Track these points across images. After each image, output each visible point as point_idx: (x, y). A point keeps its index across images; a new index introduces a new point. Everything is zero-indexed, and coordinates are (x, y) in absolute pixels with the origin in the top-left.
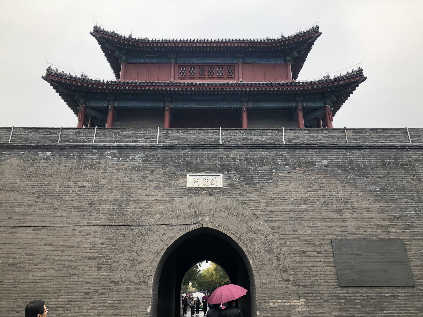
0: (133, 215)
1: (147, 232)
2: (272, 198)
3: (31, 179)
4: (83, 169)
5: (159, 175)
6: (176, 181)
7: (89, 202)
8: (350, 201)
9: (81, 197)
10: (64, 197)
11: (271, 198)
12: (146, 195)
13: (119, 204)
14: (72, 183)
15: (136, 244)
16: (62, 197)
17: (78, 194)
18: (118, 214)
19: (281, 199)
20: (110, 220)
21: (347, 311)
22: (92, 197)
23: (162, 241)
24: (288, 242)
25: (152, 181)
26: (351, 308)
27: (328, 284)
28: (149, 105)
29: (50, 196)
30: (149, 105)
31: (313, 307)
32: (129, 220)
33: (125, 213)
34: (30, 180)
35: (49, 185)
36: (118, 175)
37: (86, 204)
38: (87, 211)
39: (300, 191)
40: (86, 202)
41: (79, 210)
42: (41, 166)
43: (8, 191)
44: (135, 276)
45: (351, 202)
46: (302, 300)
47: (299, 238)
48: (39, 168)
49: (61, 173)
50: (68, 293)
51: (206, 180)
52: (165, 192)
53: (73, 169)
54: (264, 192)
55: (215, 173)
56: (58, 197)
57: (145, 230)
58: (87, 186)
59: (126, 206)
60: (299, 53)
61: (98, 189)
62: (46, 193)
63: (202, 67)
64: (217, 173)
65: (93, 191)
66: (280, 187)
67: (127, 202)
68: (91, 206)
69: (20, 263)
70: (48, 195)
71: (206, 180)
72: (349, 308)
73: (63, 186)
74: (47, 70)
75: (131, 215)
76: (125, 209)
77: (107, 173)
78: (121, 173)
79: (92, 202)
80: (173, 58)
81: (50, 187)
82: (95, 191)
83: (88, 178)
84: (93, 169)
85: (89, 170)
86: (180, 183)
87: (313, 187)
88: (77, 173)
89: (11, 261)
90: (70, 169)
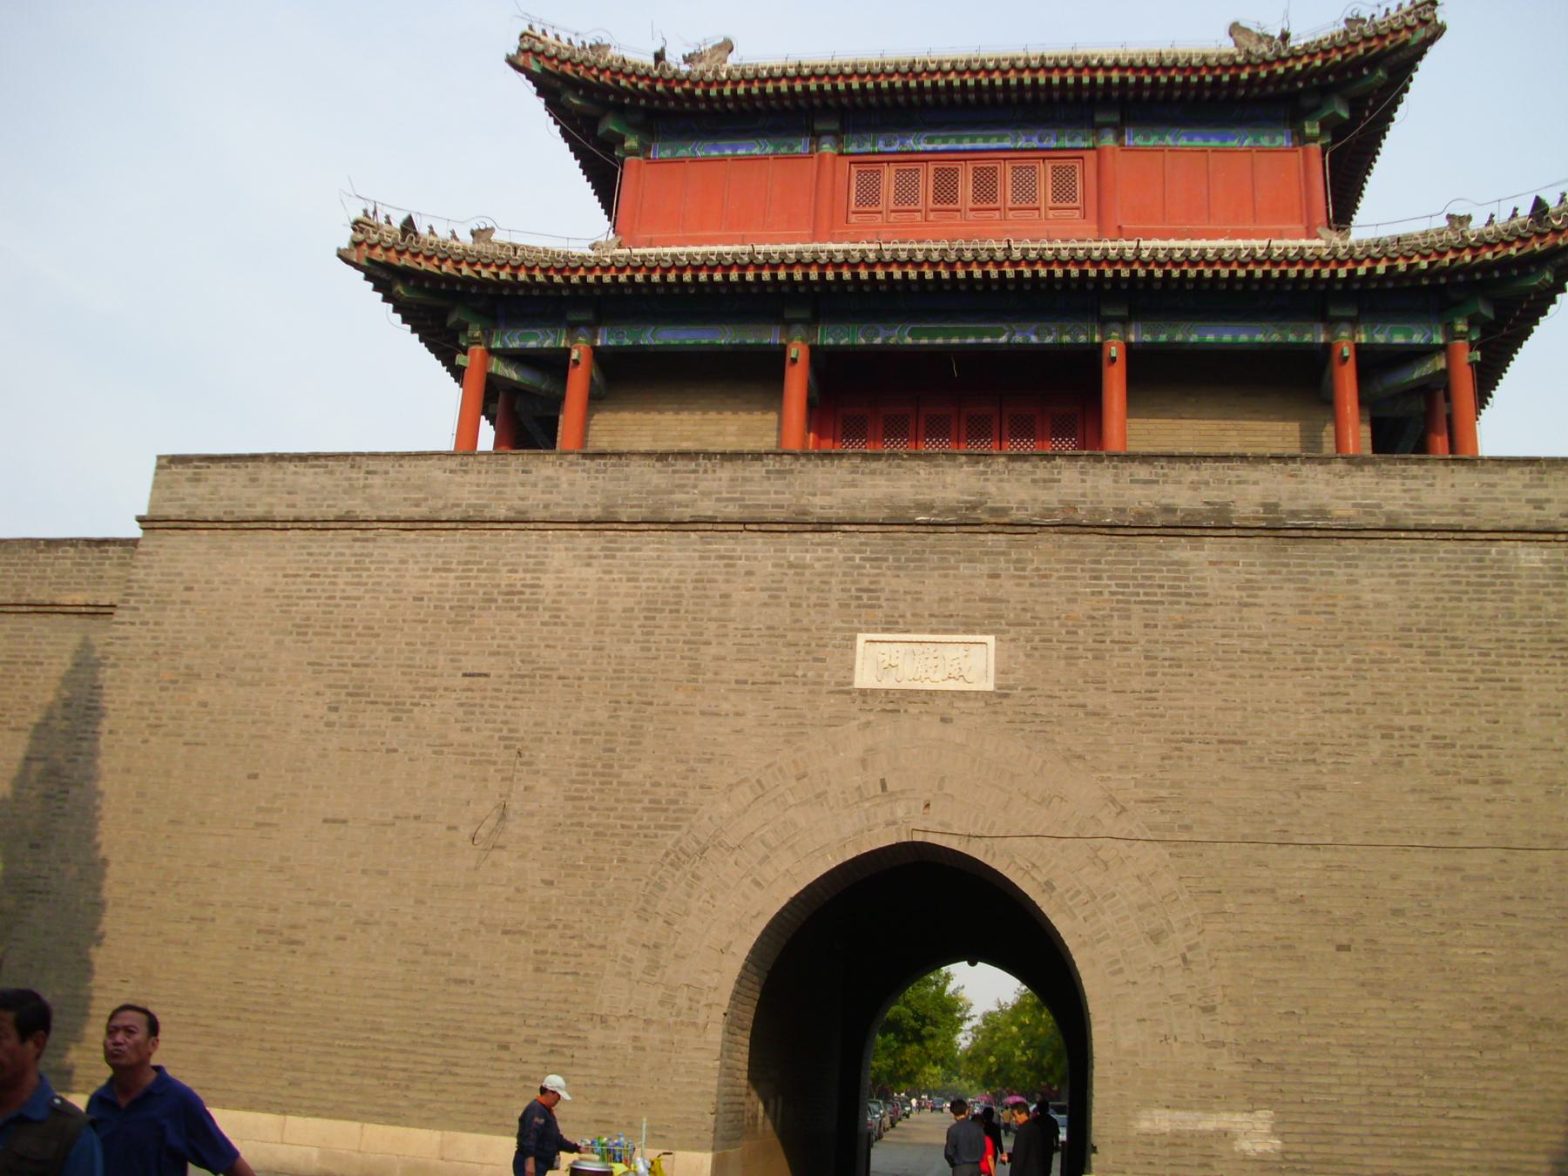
0: (656, 784)
1: (704, 850)
2: (1187, 735)
3: (311, 641)
4: (480, 608)
5: (751, 636)
6: (816, 660)
7: (501, 730)
8: (1488, 751)
9: (473, 713)
10: (416, 709)
11: (1179, 737)
12: (703, 713)
13: (606, 741)
14: (442, 660)
15: (664, 889)
16: (411, 711)
17: (463, 700)
18: (602, 779)
19: (1220, 742)
20: (574, 799)
21: (1422, 1157)
22: (512, 714)
23: (757, 884)
24: (1230, 907)
25: (724, 659)
26: (1442, 1147)
27: (1363, 1061)
28: (723, 337)
29: (372, 703)
30: (723, 337)
31: (1297, 1139)
32: (640, 801)
33: (626, 775)
34: (306, 646)
35: (367, 665)
36: (602, 633)
37: (491, 737)
38: (495, 763)
39: (1297, 713)
40: (491, 730)
41: (469, 759)
42: (338, 594)
43: (241, 683)
44: (662, 1003)
45: (1490, 756)
46: (1260, 1114)
47: (1273, 891)
48: (333, 602)
49: (404, 621)
50: (445, 1036)
51: (931, 659)
52: (772, 705)
53: (444, 608)
54: (1155, 711)
55: (965, 632)
56: (398, 709)
57: (698, 842)
58: (493, 673)
59: (629, 752)
60: (1356, 105)
61: (532, 684)
62: (357, 695)
63: (946, 165)
64: (973, 632)
65: (514, 692)
66: (1219, 692)
67: (633, 736)
68: (506, 747)
69: (294, 927)
70: (364, 699)
71: (931, 659)
72: (1433, 1147)
73: (414, 671)
74: (357, 225)
75: (648, 784)
76: (626, 762)
77: (563, 624)
78: (613, 625)
79: (511, 731)
80: (827, 133)
81: (369, 670)
82: (521, 692)
83: (496, 642)
84: (512, 609)
85: (499, 613)
86: (827, 669)
87: (1347, 694)
88: (459, 622)
89: (263, 917)
90: (436, 607)
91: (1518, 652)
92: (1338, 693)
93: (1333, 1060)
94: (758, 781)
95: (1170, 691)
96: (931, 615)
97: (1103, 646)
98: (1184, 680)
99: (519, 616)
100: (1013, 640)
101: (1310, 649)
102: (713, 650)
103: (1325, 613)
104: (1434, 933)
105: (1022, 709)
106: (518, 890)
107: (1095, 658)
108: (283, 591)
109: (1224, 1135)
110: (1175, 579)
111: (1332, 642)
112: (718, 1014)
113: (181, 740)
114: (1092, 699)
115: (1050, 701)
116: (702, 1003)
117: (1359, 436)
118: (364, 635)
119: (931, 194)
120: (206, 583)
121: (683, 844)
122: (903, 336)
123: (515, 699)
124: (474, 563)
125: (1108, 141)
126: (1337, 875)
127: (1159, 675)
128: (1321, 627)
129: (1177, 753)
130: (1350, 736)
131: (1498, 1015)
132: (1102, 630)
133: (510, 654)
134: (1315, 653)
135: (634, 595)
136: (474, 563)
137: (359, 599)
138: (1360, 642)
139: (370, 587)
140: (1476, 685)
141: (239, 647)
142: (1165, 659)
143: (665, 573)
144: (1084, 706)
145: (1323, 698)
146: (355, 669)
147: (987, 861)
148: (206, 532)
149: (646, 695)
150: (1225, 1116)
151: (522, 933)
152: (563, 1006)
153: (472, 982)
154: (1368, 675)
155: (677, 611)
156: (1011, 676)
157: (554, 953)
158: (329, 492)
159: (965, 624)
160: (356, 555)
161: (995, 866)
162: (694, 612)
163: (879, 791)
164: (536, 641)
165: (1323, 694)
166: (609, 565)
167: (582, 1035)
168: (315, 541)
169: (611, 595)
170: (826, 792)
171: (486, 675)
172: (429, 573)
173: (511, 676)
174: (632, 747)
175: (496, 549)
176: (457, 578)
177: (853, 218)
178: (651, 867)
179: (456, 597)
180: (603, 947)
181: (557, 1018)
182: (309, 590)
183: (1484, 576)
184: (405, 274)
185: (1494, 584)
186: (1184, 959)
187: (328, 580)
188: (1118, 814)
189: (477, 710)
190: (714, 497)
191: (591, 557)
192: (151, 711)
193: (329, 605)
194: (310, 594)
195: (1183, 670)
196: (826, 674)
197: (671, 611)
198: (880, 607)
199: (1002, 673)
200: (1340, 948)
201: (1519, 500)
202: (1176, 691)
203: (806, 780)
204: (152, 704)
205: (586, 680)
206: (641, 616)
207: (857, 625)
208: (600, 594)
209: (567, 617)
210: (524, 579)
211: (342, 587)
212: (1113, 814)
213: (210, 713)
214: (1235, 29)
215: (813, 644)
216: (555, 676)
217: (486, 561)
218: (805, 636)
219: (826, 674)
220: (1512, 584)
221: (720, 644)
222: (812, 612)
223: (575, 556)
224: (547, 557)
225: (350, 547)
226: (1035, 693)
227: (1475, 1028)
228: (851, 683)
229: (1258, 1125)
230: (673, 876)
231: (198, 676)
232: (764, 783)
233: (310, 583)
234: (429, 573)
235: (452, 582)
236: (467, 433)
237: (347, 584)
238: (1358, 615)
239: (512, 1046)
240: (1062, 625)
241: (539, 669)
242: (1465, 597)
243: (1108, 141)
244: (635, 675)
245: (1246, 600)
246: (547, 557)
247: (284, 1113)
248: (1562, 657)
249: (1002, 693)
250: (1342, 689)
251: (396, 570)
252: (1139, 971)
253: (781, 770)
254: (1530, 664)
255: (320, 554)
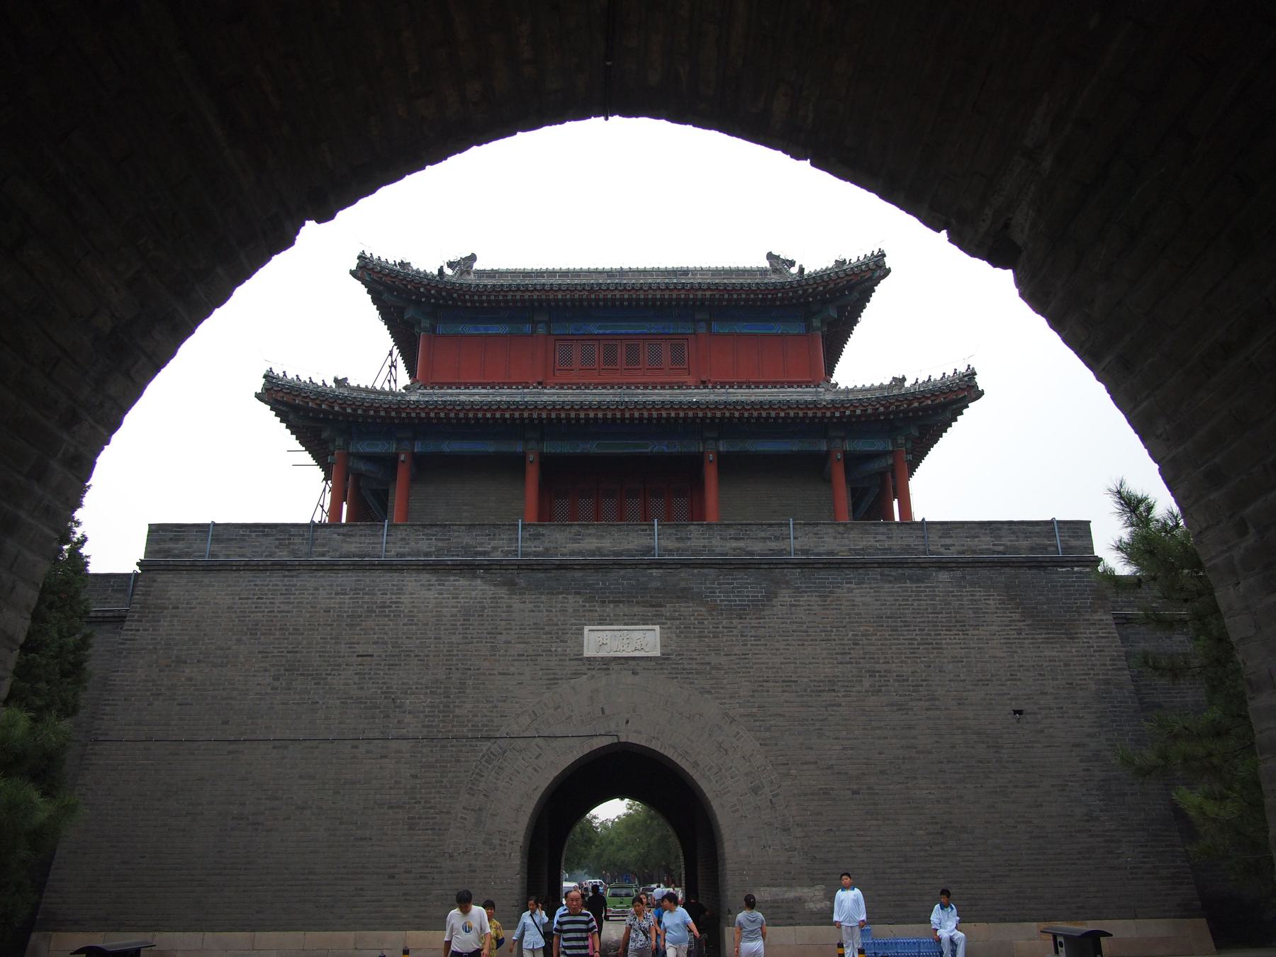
1: (505, 752)
2: (765, 678)
3: (260, 638)
6: (562, 641)
7: (382, 688)
10: (329, 677)
11: (761, 679)
12: (500, 674)
15: (483, 776)
17: (359, 671)
19: (783, 681)
25: (510, 642)
28: (490, 447)
29: (301, 675)
30: (490, 447)
32: (466, 726)
33: (458, 711)
35: (296, 652)
37: (376, 692)
39: (824, 664)
40: (375, 688)
42: (276, 610)
46: (818, 887)
47: (816, 763)
48: (273, 614)
54: (747, 665)
55: (643, 624)
57: (501, 748)
58: (375, 654)
59: (458, 698)
60: (841, 310)
62: (292, 670)
65: (389, 665)
68: (386, 698)
76: (457, 704)
77: (416, 625)
78: (445, 624)
79: (388, 688)
81: (299, 655)
82: (393, 665)
84: (385, 616)
85: (377, 619)
88: (353, 625)
91: (939, 628)
92: (845, 653)
93: (855, 855)
94: (533, 711)
95: (756, 654)
96: (624, 615)
97: (718, 630)
98: (762, 648)
99: (389, 620)
100: (669, 628)
101: (829, 629)
102: (503, 638)
103: (836, 609)
104: (903, 783)
105: (676, 666)
106: (396, 782)
107: (714, 637)
108: (238, 608)
109: (799, 900)
110: (755, 592)
111: (840, 625)
112: (517, 847)
113: (175, 703)
114: (714, 659)
115: (691, 662)
116: (508, 841)
117: (845, 517)
118: (294, 634)
119: (602, 359)
120: (187, 604)
121: (493, 750)
122: (592, 448)
123: (389, 669)
124: (360, 590)
125: (702, 330)
126: (850, 752)
127: (749, 645)
128: (834, 617)
129: (761, 688)
130: (853, 676)
131: (939, 826)
132: (717, 621)
133: (386, 643)
134: (832, 631)
135: (457, 607)
136: (360, 590)
137: (288, 612)
138: (856, 625)
139: (295, 605)
140: (918, 646)
141: (211, 643)
142: (752, 636)
143: (474, 593)
144: (709, 664)
145: (837, 656)
146: (289, 655)
147: (662, 751)
148: (185, 572)
149: (467, 664)
150: (799, 889)
151: (399, 807)
152: (427, 849)
153: (371, 839)
154: (861, 642)
155: (482, 615)
156: (669, 648)
157: (419, 818)
158: (267, 547)
159: (643, 620)
160: (286, 585)
161: (666, 754)
162: (492, 616)
163: (601, 715)
164: (400, 635)
165: (838, 654)
166: (441, 590)
167: (438, 865)
168: (258, 577)
169: (443, 607)
170: (571, 716)
171: (371, 656)
172: (333, 596)
173: (386, 656)
174: (460, 695)
175: (373, 581)
176: (350, 598)
177: (557, 373)
178: (475, 763)
179: (350, 610)
180: (448, 813)
181: (423, 856)
182: (256, 607)
183: (920, 587)
184: (295, 408)
185: (926, 591)
186: (771, 802)
187: (268, 601)
188: (731, 723)
189: (367, 677)
190: (500, 550)
191: (430, 585)
192: (153, 685)
193: (270, 616)
194: (257, 610)
195: (762, 642)
196: (568, 649)
197: (479, 616)
198: (596, 611)
199: (664, 646)
200: (854, 793)
201: (937, 545)
202: (758, 654)
203: (559, 709)
204: (154, 681)
205: (431, 657)
206: (462, 619)
207: (584, 622)
208: (437, 607)
209: (418, 620)
210: (391, 599)
211: (278, 605)
212: (728, 723)
213: (195, 685)
214: (770, 256)
215: (560, 632)
216: (413, 655)
217: (367, 589)
218: (556, 628)
219: (568, 649)
220: (935, 591)
221: (507, 634)
222: (559, 614)
223: (421, 585)
224: (404, 585)
225: (282, 581)
226: (682, 657)
227: (929, 834)
228: (582, 654)
229: (817, 893)
230: (488, 768)
231: (185, 662)
232: (537, 712)
233: (258, 603)
234: (333, 596)
235: (347, 601)
236: (335, 511)
237: (281, 603)
238: (853, 609)
239: (397, 876)
240: (695, 619)
241: (403, 651)
242: (910, 599)
243: (702, 330)
244: (460, 653)
245: (793, 603)
246: (404, 585)
247: (254, 931)
248: (963, 631)
249: (665, 657)
250: (847, 651)
251: (312, 594)
252: (747, 810)
253: (545, 704)
254: (946, 635)
255: (262, 585)
